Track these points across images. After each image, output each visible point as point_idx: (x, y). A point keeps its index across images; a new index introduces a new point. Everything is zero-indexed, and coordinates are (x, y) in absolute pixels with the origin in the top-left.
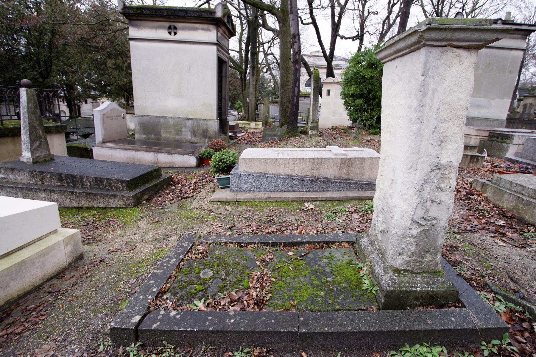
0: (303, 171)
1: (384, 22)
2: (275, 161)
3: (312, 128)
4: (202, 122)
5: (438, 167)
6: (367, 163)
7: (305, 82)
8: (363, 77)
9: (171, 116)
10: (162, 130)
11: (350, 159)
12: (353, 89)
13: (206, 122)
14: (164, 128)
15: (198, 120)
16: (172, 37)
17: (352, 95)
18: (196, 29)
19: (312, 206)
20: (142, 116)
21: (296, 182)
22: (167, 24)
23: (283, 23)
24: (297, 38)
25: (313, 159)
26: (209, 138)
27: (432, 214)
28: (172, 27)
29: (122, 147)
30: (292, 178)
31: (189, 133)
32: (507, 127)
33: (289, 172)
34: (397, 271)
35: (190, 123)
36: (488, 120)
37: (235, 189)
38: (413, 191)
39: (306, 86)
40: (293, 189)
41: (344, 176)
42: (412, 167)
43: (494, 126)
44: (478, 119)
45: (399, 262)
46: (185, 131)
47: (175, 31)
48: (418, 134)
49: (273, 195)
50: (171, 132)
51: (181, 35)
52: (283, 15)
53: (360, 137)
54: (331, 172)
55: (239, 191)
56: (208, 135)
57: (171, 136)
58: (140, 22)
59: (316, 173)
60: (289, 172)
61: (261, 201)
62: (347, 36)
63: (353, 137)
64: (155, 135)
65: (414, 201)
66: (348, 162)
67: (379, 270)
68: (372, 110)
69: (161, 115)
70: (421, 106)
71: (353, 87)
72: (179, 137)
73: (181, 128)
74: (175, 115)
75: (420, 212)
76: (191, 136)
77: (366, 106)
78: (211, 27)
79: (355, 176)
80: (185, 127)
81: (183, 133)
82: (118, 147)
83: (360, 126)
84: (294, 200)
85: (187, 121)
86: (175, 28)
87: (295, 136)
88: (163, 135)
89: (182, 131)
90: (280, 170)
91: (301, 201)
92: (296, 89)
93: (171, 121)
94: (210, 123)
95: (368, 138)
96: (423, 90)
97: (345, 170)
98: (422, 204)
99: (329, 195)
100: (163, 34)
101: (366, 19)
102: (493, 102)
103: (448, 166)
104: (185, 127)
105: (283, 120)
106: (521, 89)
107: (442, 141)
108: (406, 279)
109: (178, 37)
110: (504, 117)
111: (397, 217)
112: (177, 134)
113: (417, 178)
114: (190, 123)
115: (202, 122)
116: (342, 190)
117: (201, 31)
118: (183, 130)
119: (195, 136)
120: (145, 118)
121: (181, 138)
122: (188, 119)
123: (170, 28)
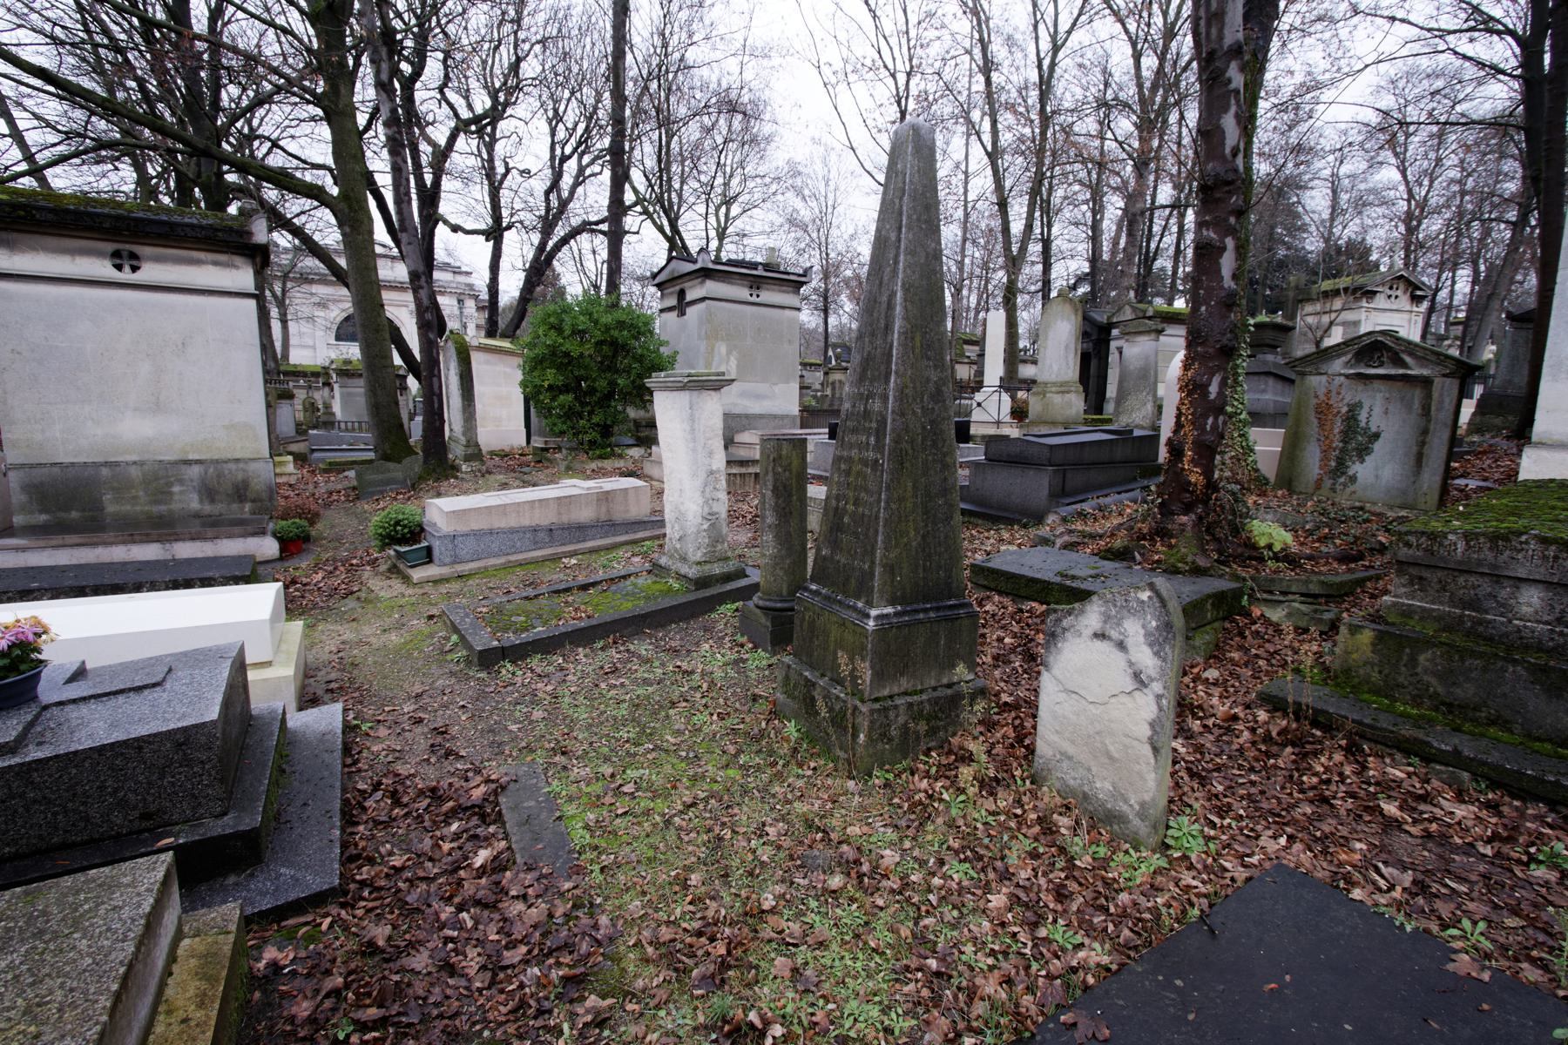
0: (545, 518)
1: (547, 193)
2: (503, 509)
3: (468, 459)
4: (232, 466)
5: (712, 473)
6: (631, 494)
7: (335, 327)
8: (567, 354)
9: (134, 458)
10: (107, 497)
11: (608, 492)
12: (551, 376)
13: (241, 465)
14: (113, 489)
15: (217, 461)
16: (126, 276)
17: (550, 387)
18: (198, 262)
19: (574, 561)
20: (32, 466)
21: (541, 535)
22: (110, 247)
23: (352, 227)
24: (423, 279)
25: (559, 498)
26: (253, 501)
27: (715, 509)
28: (125, 254)
29: (54, 542)
30: (535, 530)
31: (195, 497)
32: (802, 427)
33: (526, 522)
34: (699, 563)
35: (195, 471)
36: (775, 417)
37: (447, 560)
38: (698, 494)
39: (338, 338)
40: (537, 545)
41: (603, 518)
42: (694, 475)
43: (783, 427)
44: (761, 416)
45: (699, 556)
46: (181, 492)
47: (134, 263)
48: (694, 450)
49: (513, 558)
50: (135, 498)
51: (151, 272)
52: (350, 207)
53: (577, 465)
54: (585, 514)
55: (454, 563)
56: (250, 495)
57: (138, 508)
58: (15, 235)
59: (565, 519)
60: (526, 522)
61: (498, 568)
62: (468, 227)
63: (563, 468)
64: (84, 510)
65: (701, 501)
66: (606, 497)
67: (684, 570)
68: (591, 413)
69: (100, 459)
70: (693, 430)
71: (551, 373)
72: (163, 508)
73: (169, 484)
74: (146, 457)
75: (706, 510)
76: (201, 501)
77: (578, 407)
78: (238, 260)
79: (619, 515)
80: (181, 482)
81: (176, 497)
82: (42, 543)
83: (574, 444)
84: (545, 560)
85: (183, 467)
86: (133, 256)
87: (447, 478)
88: (111, 508)
89: (171, 494)
90: (512, 521)
91: (555, 559)
92: (435, 380)
93: (135, 472)
94: (253, 466)
95: (593, 465)
96: (692, 419)
97: (604, 509)
98: (706, 502)
99: (590, 544)
100: (102, 268)
101: (501, 182)
102: (777, 389)
103: (718, 471)
104: (181, 482)
105: (387, 446)
106: (835, 346)
107: (711, 454)
108: (707, 567)
109: (141, 276)
110: (795, 410)
111: (691, 518)
112: (157, 502)
113: (699, 482)
114: (195, 471)
115: (232, 466)
116: (606, 536)
117: (211, 268)
118: (176, 489)
119: (212, 501)
120: (45, 470)
121: (170, 511)
122: (188, 462)
123: (116, 255)
